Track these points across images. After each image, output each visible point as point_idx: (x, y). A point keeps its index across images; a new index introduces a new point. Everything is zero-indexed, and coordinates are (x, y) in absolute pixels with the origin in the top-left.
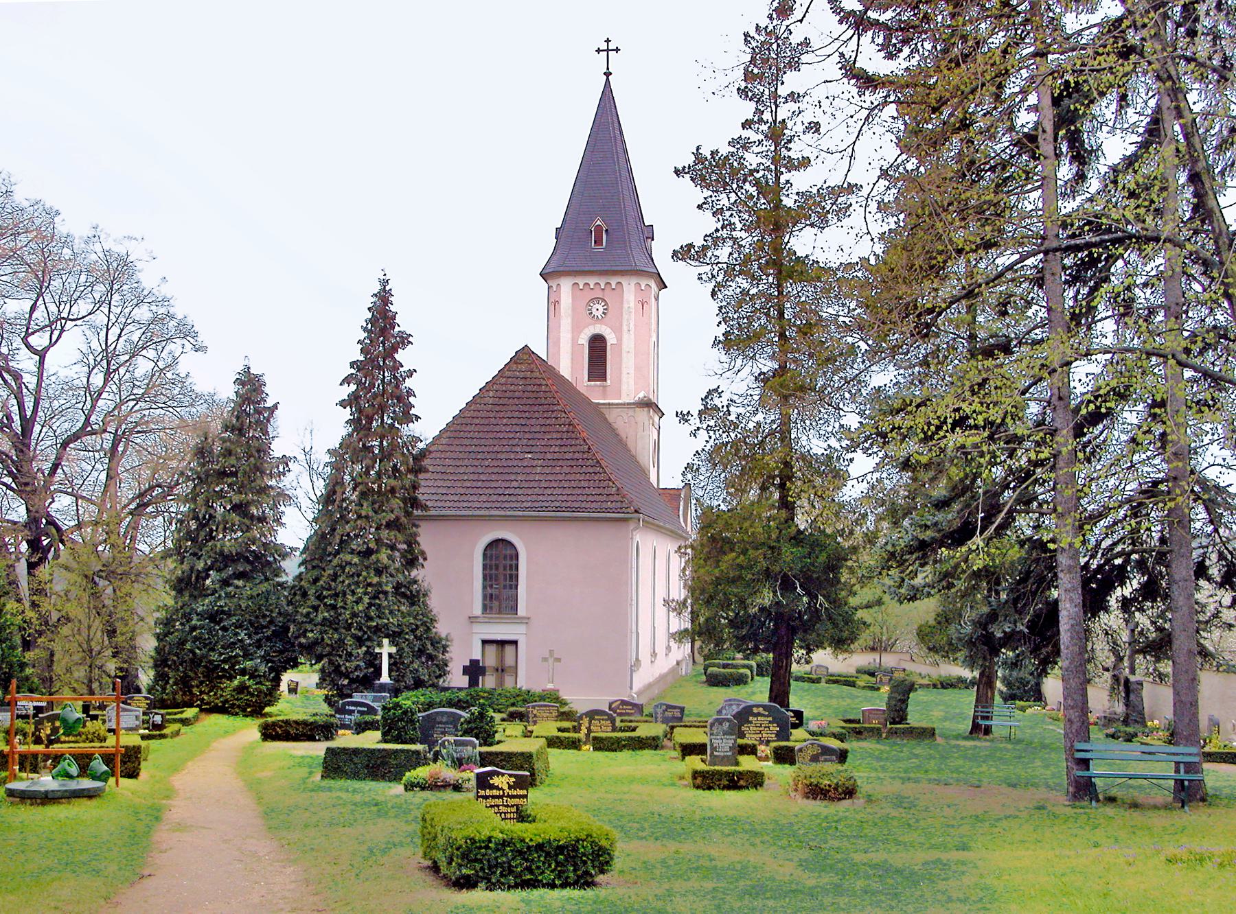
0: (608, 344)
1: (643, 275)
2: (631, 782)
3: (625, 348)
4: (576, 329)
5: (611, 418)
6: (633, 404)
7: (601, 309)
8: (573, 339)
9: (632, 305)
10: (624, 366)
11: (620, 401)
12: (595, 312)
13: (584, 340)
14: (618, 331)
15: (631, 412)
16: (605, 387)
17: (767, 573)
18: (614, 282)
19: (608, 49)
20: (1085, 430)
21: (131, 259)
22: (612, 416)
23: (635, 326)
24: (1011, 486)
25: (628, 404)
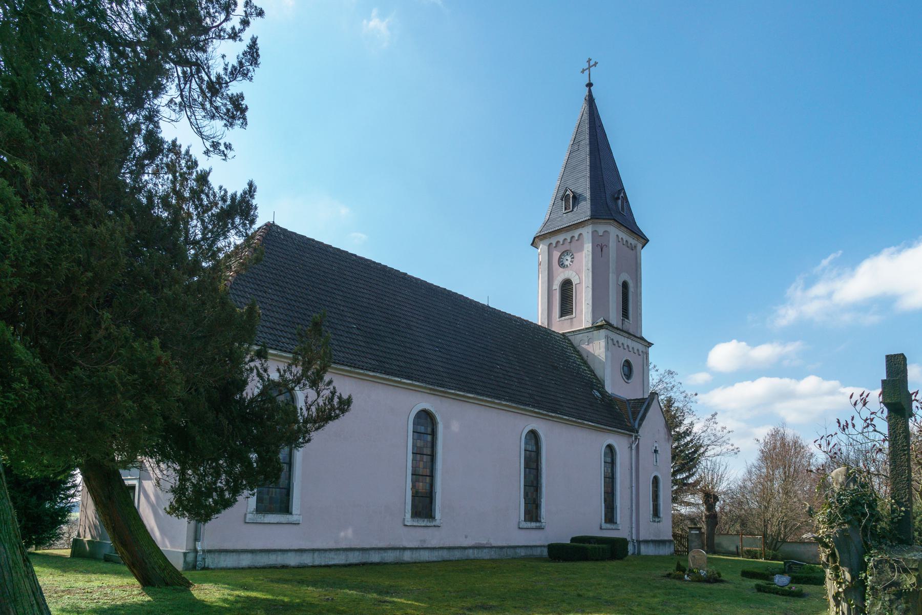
5: (575, 343)
6: (591, 328)
12: (567, 263)
13: (556, 286)
14: (578, 273)
18: (576, 233)
19: (591, 65)
22: (576, 340)
25: (587, 329)
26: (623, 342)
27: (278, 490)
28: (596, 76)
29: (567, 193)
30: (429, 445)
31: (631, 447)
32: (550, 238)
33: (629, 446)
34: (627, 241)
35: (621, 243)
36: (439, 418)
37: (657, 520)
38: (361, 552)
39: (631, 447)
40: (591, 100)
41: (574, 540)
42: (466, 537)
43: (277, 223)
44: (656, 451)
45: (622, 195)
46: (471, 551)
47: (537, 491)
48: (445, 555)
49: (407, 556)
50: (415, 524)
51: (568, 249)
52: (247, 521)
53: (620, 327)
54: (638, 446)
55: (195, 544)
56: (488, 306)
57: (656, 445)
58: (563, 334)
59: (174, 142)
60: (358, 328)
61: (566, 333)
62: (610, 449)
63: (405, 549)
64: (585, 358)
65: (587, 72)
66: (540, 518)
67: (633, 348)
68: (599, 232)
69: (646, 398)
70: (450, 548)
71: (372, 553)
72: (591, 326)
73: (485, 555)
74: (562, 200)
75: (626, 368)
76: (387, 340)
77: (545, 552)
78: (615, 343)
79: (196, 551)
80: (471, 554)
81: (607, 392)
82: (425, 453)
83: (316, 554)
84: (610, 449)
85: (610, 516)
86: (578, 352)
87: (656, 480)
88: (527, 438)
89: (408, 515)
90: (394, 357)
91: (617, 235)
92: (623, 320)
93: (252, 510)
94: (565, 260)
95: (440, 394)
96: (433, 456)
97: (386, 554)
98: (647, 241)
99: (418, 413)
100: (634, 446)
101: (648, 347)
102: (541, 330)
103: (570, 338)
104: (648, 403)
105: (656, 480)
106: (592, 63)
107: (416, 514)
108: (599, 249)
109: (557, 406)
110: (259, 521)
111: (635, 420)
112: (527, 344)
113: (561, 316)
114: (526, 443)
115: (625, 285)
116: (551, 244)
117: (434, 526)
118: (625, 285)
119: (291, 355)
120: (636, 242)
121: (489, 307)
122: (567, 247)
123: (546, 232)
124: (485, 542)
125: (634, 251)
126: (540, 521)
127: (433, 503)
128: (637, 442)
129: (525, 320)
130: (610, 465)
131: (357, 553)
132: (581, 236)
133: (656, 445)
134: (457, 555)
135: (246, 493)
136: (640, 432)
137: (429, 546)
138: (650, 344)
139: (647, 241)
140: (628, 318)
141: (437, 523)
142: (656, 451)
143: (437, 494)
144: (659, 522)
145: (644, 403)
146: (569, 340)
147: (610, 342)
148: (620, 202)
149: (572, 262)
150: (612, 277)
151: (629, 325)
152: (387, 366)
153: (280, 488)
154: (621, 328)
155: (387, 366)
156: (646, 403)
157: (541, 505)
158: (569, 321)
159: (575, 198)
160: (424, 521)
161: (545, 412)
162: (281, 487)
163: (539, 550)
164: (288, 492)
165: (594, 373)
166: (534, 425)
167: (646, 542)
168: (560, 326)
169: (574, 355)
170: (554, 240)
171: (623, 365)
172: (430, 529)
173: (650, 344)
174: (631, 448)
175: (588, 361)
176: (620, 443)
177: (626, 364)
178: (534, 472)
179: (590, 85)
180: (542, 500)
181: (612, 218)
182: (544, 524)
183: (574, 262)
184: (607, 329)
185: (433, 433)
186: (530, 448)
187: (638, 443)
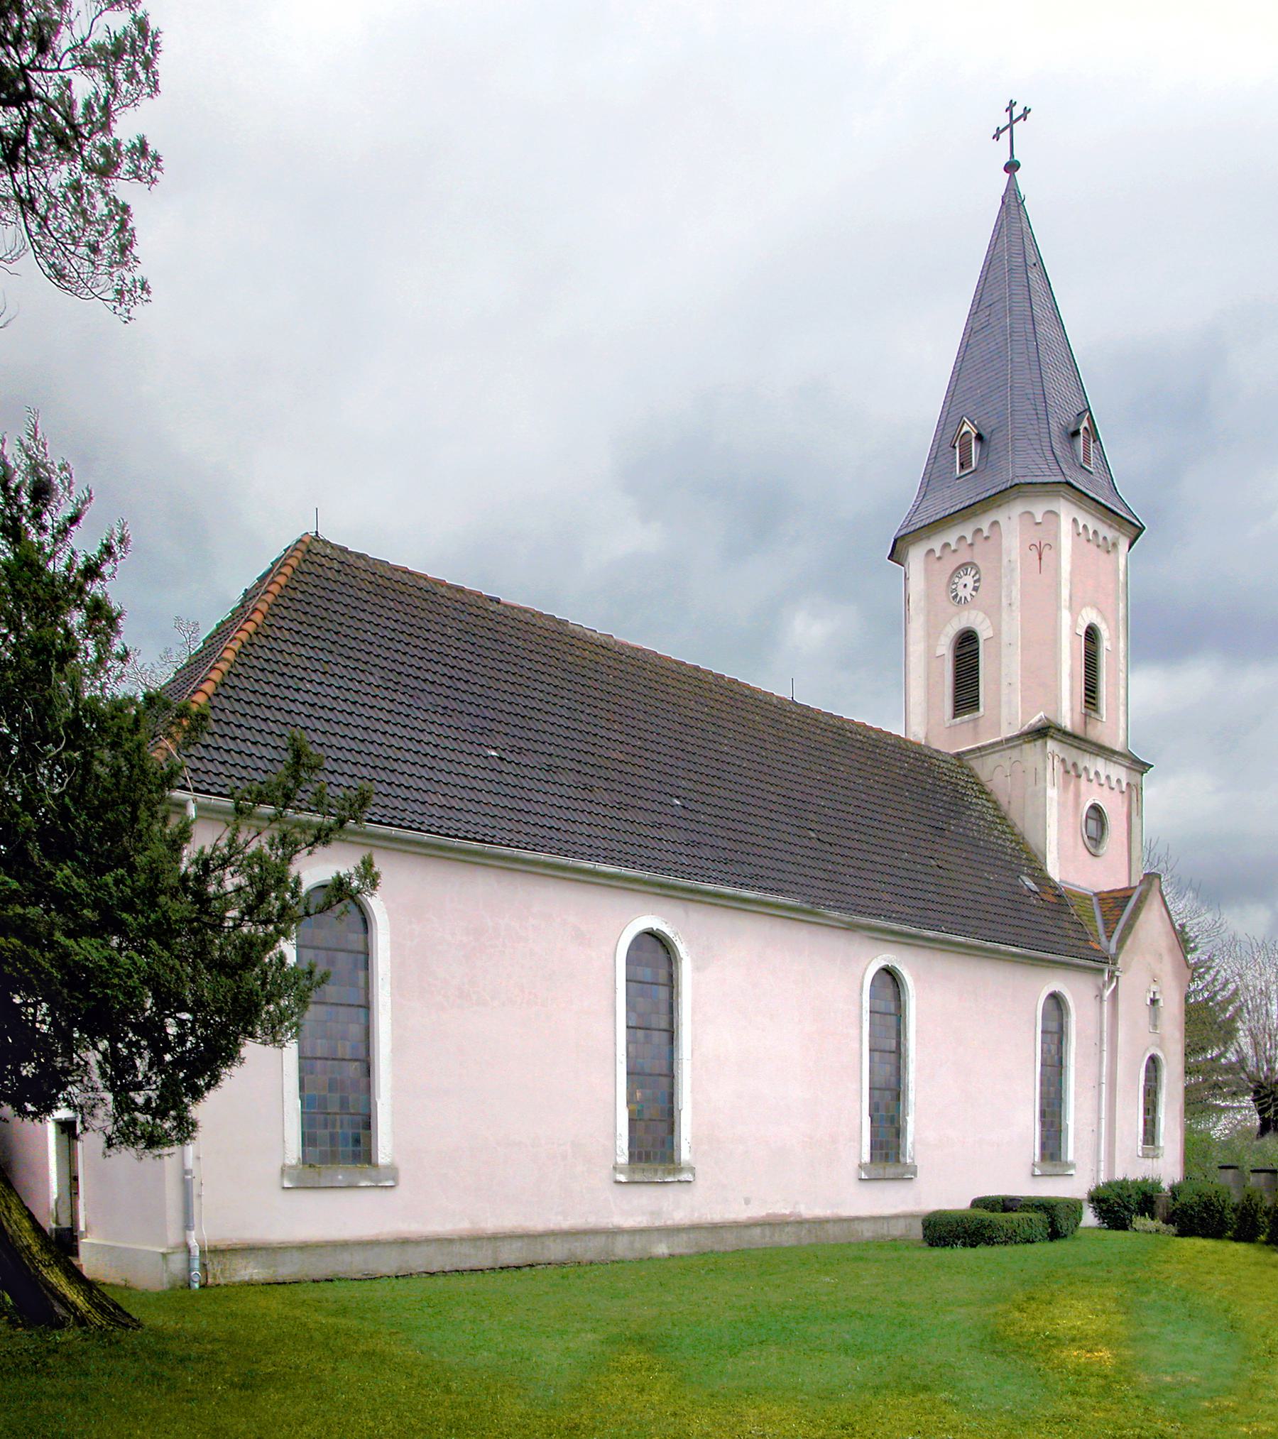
0: (981, 641)
1: (1036, 495)
2: (1085, 899)
3: (1005, 638)
4: (932, 634)
5: (983, 775)
6: (1018, 737)
7: (970, 586)
9: (1015, 555)
10: (1004, 671)
11: (998, 739)
12: (962, 593)
13: (945, 648)
15: (1015, 754)
16: (976, 720)
17: (90, 223)
18: (984, 523)
19: (1016, 115)
20: (154, 1009)
22: (986, 770)
23: (1023, 593)
25: (1008, 740)
27: (346, 1117)
29: (965, 428)
30: (664, 1008)
31: (1100, 997)
34: (1095, 532)
35: (1083, 537)
36: (681, 948)
37: (1151, 1153)
38: (526, 1240)
39: (1100, 997)
40: (1012, 203)
42: (747, 1201)
43: (324, 535)
44: (1154, 1001)
45: (1085, 424)
46: (758, 1231)
47: (898, 1099)
50: (638, 1177)
51: (968, 560)
53: (1079, 731)
55: (185, 1236)
56: (793, 702)
58: (958, 756)
60: (683, 807)
61: (963, 753)
62: (1056, 1000)
64: (1005, 806)
65: (1005, 136)
67: (1108, 777)
68: (1036, 516)
69: (1135, 887)
71: (549, 1242)
74: (954, 447)
75: (1092, 824)
77: (917, 1231)
78: (1070, 767)
81: (1049, 879)
82: (653, 1026)
84: (1056, 1000)
88: (876, 984)
91: (1075, 520)
92: (1086, 715)
94: (960, 587)
95: (684, 895)
96: (671, 1033)
97: (577, 1244)
100: (1107, 993)
103: (973, 763)
106: (1018, 111)
111: (1109, 937)
113: (955, 716)
116: (932, 551)
119: (228, 804)
120: (1117, 534)
122: (964, 557)
124: (787, 1212)
125: (1112, 555)
127: (676, 1133)
128: (1114, 984)
130: (894, 1018)
131: (517, 1244)
133: (1154, 987)
136: (1119, 961)
139: (1142, 529)
140: (1096, 711)
143: (683, 1113)
144: (1156, 1157)
145: (1129, 897)
146: (971, 769)
153: (351, 1114)
156: (1134, 898)
158: (971, 725)
159: (979, 437)
160: (656, 1171)
161: (914, 930)
162: (352, 1111)
166: (891, 956)
170: (936, 544)
171: (1087, 817)
172: (669, 1187)
174: (1101, 997)
177: (1093, 814)
178: (660, 1038)
179: (1012, 167)
180: (909, 1119)
183: (980, 590)
185: (671, 983)
186: (881, 1006)
187: (1116, 988)
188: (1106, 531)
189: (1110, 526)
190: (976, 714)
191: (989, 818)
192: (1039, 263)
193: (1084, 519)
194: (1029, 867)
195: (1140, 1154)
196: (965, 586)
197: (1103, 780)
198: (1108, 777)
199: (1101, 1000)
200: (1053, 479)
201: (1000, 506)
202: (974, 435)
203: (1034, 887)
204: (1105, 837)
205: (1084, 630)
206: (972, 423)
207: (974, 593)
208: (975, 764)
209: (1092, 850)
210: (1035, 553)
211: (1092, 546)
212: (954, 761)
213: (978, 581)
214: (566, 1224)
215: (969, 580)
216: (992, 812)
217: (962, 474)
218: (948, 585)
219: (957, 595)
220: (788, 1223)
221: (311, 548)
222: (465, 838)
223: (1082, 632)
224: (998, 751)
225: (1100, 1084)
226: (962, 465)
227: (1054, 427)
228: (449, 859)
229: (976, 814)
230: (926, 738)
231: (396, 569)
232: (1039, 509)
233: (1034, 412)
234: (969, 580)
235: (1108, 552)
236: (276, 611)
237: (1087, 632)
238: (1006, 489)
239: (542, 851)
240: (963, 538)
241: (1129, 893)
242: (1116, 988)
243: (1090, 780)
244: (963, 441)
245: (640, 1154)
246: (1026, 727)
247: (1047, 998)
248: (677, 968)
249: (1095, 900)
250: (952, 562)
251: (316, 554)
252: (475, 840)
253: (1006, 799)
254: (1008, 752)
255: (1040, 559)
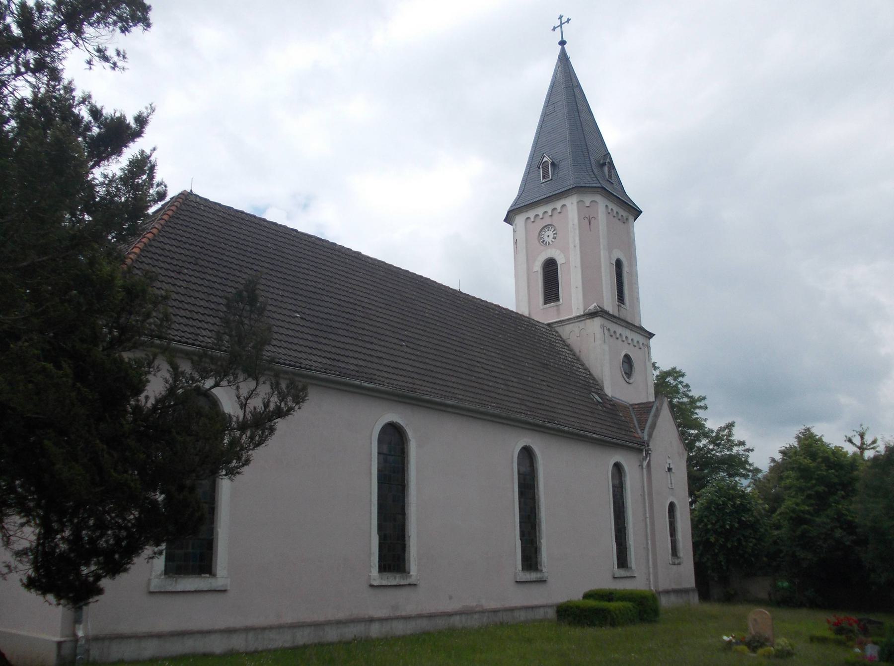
0: (559, 265)
6: (583, 316)
7: (551, 236)
8: (528, 269)
11: (572, 316)
12: (547, 239)
13: (538, 267)
15: (581, 325)
16: (558, 306)
18: (558, 205)
19: (563, 22)
21: (4, 547)
22: (566, 332)
24: (74, 219)
25: (577, 317)
26: (620, 332)
28: (569, 32)
29: (545, 159)
31: (641, 466)
32: (526, 211)
33: (639, 464)
37: (677, 562)
38: (313, 628)
40: (564, 60)
41: (587, 596)
43: (195, 192)
44: (670, 469)
46: (458, 618)
48: (424, 624)
49: (375, 630)
50: (384, 583)
52: (152, 589)
53: (616, 314)
54: (649, 464)
55: (74, 628)
56: (460, 292)
57: (669, 461)
58: (549, 325)
59: (70, 83)
62: (618, 467)
63: (371, 620)
66: (541, 565)
67: (632, 340)
70: (431, 616)
72: (582, 313)
73: (474, 622)
74: (539, 168)
75: (626, 365)
76: (340, 332)
77: (551, 614)
79: (76, 640)
80: (456, 621)
81: (606, 395)
83: (251, 635)
84: (618, 467)
85: (622, 561)
86: (568, 346)
87: (672, 506)
89: (375, 572)
90: (351, 354)
92: (619, 306)
93: (159, 573)
98: (640, 212)
99: (381, 430)
100: (645, 464)
101: (650, 338)
102: (523, 320)
103: (557, 329)
104: (657, 408)
105: (672, 506)
106: (564, 19)
107: (384, 567)
108: (588, 220)
109: (555, 415)
110: (170, 589)
111: (643, 430)
112: (510, 337)
113: (545, 303)
114: (519, 464)
115: (619, 264)
116: (528, 218)
117: (410, 585)
118: (619, 264)
121: (462, 293)
122: (547, 221)
123: (522, 205)
124: (475, 604)
126: (541, 571)
128: (648, 458)
129: (504, 309)
131: (307, 631)
132: (564, 207)
133: (669, 461)
134: (441, 623)
135: (148, 550)
137: (404, 614)
138: (651, 335)
139: (640, 212)
140: (623, 304)
141: (412, 580)
142: (670, 469)
144: (679, 564)
145: (651, 407)
146: (557, 332)
147: (606, 332)
148: (606, 169)
149: (554, 238)
150: (603, 254)
151: (625, 314)
152: (343, 365)
154: (617, 316)
155: (343, 365)
157: (540, 548)
158: (555, 308)
159: (553, 164)
160: (395, 578)
163: (542, 611)
164: (209, 546)
165: (589, 372)
167: (667, 592)
168: (544, 315)
169: (564, 350)
170: (531, 214)
173: (651, 335)
174: (642, 466)
175: (581, 356)
176: (629, 462)
179: (563, 43)
180: (542, 541)
181: (599, 185)
182: (546, 574)
184: (602, 317)
187: (650, 460)
188: (622, 212)
189: (624, 210)
190: (558, 303)
191: (570, 359)
192: (579, 86)
193: (611, 206)
194: (595, 388)
195: (671, 562)
196: (548, 236)
197: (630, 341)
198: (632, 340)
199: (642, 468)
200: (595, 185)
201: (566, 197)
202: (550, 163)
203: (600, 400)
204: (633, 372)
205: (615, 261)
206: (549, 157)
207: (553, 240)
208: (560, 329)
209: (627, 380)
210: (587, 221)
211: (616, 220)
212: (547, 327)
213: (556, 234)
214: (341, 615)
215: (551, 233)
216: (571, 356)
217: (544, 181)
218: (539, 236)
219: (544, 241)
220: (476, 613)
221: (188, 197)
222: (284, 364)
223: (614, 262)
224: (572, 323)
225: (646, 518)
226: (544, 178)
227: (593, 161)
228: (485, 420)
229: (563, 357)
230: (529, 314)
231: (237, 211)
232: (588, 200)
233: (582, 153)
234: (551, 233)
235: (624, 223)
236: (167, 229)
237: (616, 263)
238: (569, 189)
239: (330, 373)
240: (546, 212)
241: (650, 405)
242: (650, 460)
243: (623, 341)
244: (544, 165)
245: (385, 565)
246: (587, 311)
247: (613, 466)
248: (407, 446)
249: (631, 408)
250: (540, 224)
251: (191, 201)
252: (289, 365)
253: (578, 350)
254: (577, 324)
255: (590, 224)
